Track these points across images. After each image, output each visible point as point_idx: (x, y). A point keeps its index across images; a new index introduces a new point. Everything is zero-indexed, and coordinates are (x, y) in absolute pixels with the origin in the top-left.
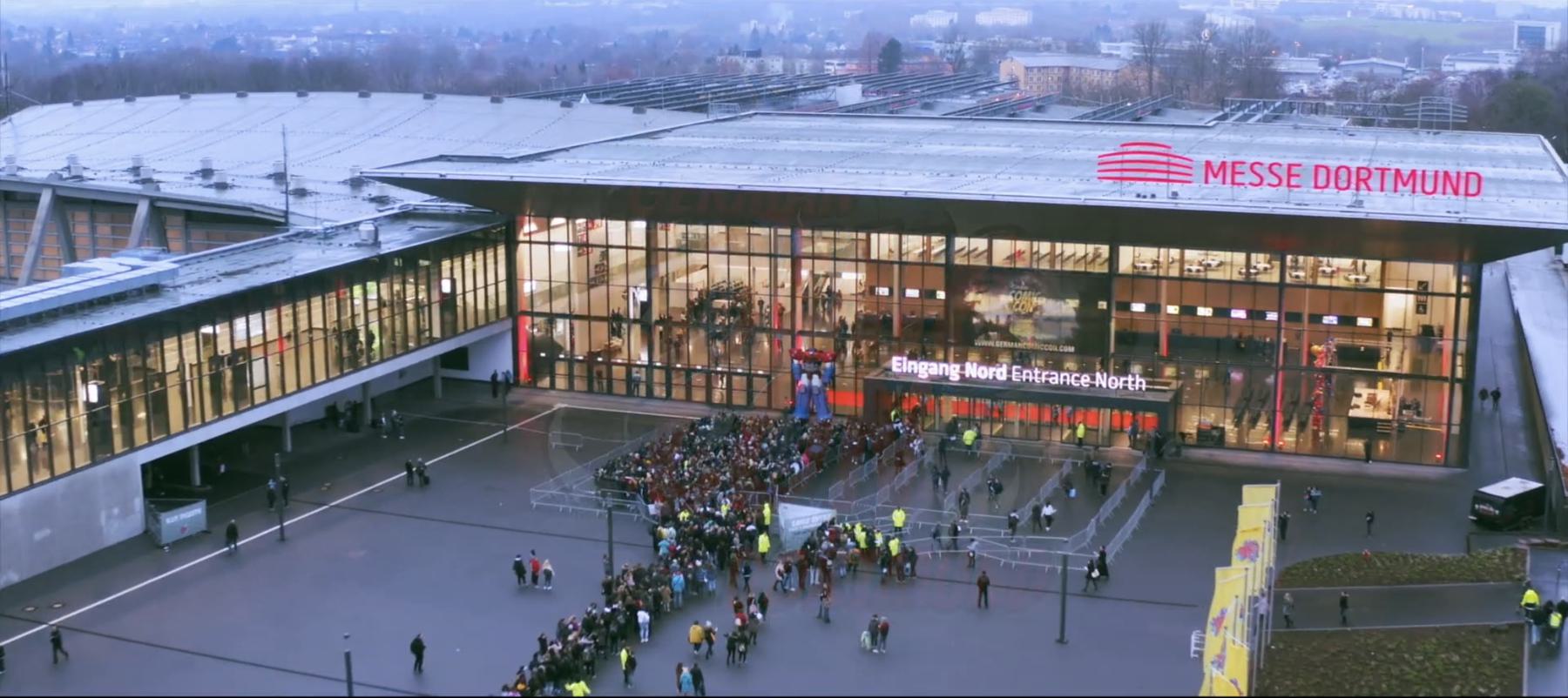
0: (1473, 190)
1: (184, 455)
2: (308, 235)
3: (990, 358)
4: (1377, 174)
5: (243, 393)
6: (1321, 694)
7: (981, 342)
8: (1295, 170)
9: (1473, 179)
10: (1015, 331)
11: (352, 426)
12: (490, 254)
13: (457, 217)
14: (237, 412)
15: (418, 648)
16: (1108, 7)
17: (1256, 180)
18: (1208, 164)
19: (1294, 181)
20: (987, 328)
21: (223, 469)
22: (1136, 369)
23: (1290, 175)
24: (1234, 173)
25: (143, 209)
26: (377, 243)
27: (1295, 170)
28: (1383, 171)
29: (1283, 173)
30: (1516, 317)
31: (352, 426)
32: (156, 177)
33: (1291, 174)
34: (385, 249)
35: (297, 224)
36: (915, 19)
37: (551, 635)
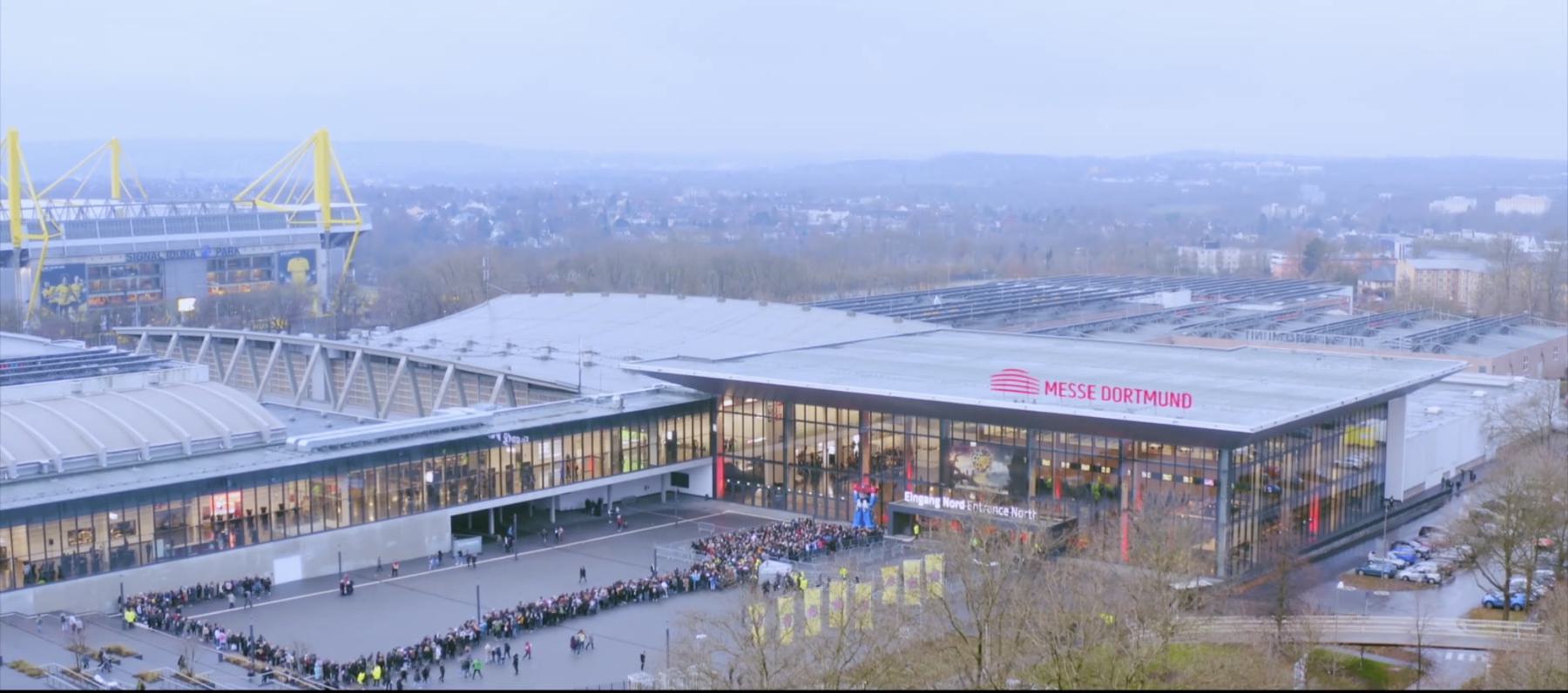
1: (486, 512)
2: (590, 400)
3: (961, 495)
5: (529, 484)
6: (1082, 688)
7: (958, 486)
10: (977, 480)
11: (598, 513)
12: (697, 422)
13: (687, 394)
14: (523, 491)
15: (643, 657)
20: (962, 477)
25: (500, 380)
26: (622, 407)
29: (1085, 389)
31: (598, 513)
32: (258, 405)
33: (1126, 395)
34: (626, 410)
35: (586, 394)
36: (1435, 204)
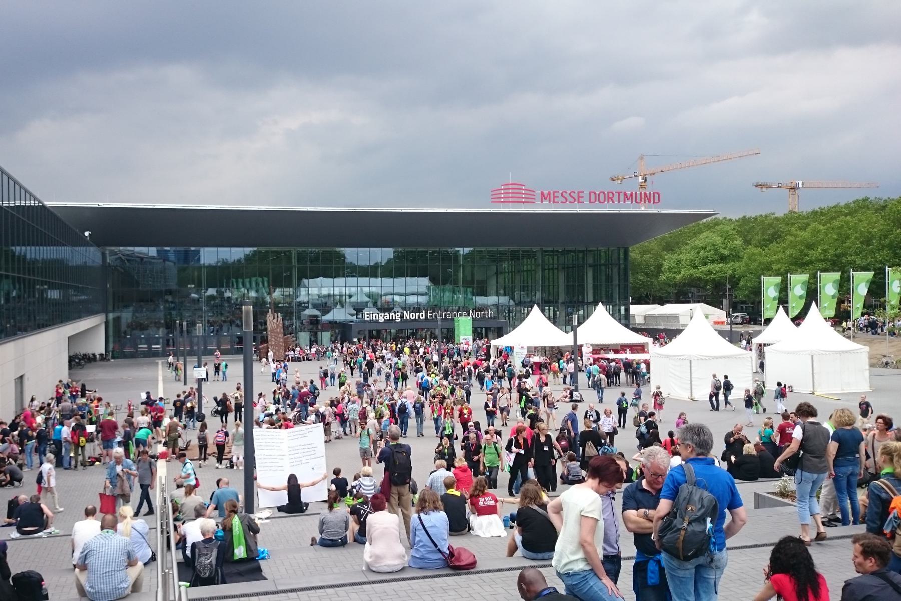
0: (656, 200)
4: (616, 195)
8: (581, 195)
9: (656, 195)
16: (832, 326)
17: (564, 200)
18: (542, 194)
19: (581, 200)
21: (87, 234)
22: (755, 453)
23: (579, 197)
24: (554, 197)
27: (581, 195)
28: (619, 193)
29: (575, 196)
30: (836, 352)
32: (449, 572)
37: (294, 384)
